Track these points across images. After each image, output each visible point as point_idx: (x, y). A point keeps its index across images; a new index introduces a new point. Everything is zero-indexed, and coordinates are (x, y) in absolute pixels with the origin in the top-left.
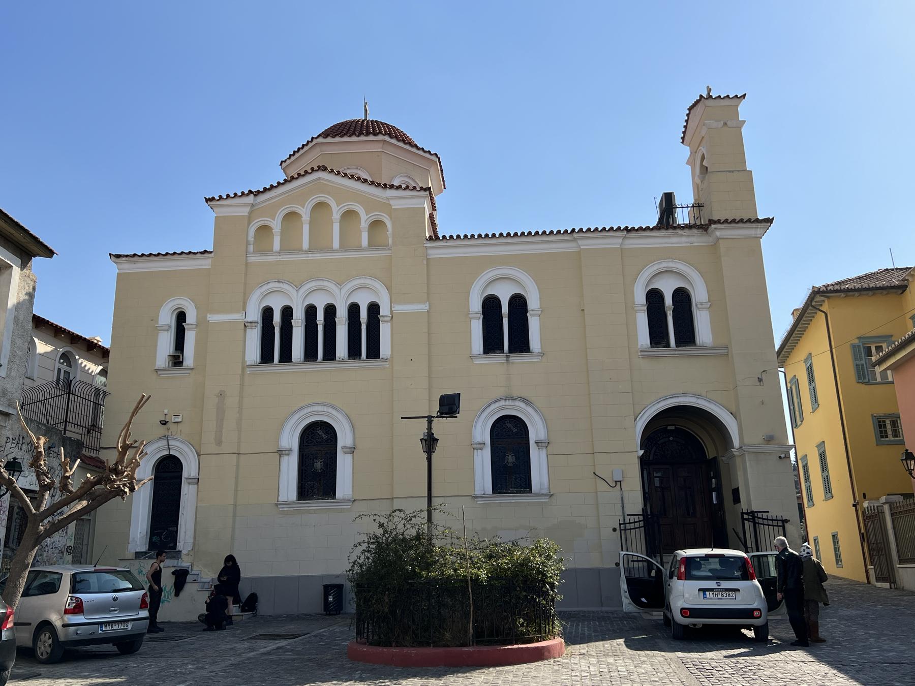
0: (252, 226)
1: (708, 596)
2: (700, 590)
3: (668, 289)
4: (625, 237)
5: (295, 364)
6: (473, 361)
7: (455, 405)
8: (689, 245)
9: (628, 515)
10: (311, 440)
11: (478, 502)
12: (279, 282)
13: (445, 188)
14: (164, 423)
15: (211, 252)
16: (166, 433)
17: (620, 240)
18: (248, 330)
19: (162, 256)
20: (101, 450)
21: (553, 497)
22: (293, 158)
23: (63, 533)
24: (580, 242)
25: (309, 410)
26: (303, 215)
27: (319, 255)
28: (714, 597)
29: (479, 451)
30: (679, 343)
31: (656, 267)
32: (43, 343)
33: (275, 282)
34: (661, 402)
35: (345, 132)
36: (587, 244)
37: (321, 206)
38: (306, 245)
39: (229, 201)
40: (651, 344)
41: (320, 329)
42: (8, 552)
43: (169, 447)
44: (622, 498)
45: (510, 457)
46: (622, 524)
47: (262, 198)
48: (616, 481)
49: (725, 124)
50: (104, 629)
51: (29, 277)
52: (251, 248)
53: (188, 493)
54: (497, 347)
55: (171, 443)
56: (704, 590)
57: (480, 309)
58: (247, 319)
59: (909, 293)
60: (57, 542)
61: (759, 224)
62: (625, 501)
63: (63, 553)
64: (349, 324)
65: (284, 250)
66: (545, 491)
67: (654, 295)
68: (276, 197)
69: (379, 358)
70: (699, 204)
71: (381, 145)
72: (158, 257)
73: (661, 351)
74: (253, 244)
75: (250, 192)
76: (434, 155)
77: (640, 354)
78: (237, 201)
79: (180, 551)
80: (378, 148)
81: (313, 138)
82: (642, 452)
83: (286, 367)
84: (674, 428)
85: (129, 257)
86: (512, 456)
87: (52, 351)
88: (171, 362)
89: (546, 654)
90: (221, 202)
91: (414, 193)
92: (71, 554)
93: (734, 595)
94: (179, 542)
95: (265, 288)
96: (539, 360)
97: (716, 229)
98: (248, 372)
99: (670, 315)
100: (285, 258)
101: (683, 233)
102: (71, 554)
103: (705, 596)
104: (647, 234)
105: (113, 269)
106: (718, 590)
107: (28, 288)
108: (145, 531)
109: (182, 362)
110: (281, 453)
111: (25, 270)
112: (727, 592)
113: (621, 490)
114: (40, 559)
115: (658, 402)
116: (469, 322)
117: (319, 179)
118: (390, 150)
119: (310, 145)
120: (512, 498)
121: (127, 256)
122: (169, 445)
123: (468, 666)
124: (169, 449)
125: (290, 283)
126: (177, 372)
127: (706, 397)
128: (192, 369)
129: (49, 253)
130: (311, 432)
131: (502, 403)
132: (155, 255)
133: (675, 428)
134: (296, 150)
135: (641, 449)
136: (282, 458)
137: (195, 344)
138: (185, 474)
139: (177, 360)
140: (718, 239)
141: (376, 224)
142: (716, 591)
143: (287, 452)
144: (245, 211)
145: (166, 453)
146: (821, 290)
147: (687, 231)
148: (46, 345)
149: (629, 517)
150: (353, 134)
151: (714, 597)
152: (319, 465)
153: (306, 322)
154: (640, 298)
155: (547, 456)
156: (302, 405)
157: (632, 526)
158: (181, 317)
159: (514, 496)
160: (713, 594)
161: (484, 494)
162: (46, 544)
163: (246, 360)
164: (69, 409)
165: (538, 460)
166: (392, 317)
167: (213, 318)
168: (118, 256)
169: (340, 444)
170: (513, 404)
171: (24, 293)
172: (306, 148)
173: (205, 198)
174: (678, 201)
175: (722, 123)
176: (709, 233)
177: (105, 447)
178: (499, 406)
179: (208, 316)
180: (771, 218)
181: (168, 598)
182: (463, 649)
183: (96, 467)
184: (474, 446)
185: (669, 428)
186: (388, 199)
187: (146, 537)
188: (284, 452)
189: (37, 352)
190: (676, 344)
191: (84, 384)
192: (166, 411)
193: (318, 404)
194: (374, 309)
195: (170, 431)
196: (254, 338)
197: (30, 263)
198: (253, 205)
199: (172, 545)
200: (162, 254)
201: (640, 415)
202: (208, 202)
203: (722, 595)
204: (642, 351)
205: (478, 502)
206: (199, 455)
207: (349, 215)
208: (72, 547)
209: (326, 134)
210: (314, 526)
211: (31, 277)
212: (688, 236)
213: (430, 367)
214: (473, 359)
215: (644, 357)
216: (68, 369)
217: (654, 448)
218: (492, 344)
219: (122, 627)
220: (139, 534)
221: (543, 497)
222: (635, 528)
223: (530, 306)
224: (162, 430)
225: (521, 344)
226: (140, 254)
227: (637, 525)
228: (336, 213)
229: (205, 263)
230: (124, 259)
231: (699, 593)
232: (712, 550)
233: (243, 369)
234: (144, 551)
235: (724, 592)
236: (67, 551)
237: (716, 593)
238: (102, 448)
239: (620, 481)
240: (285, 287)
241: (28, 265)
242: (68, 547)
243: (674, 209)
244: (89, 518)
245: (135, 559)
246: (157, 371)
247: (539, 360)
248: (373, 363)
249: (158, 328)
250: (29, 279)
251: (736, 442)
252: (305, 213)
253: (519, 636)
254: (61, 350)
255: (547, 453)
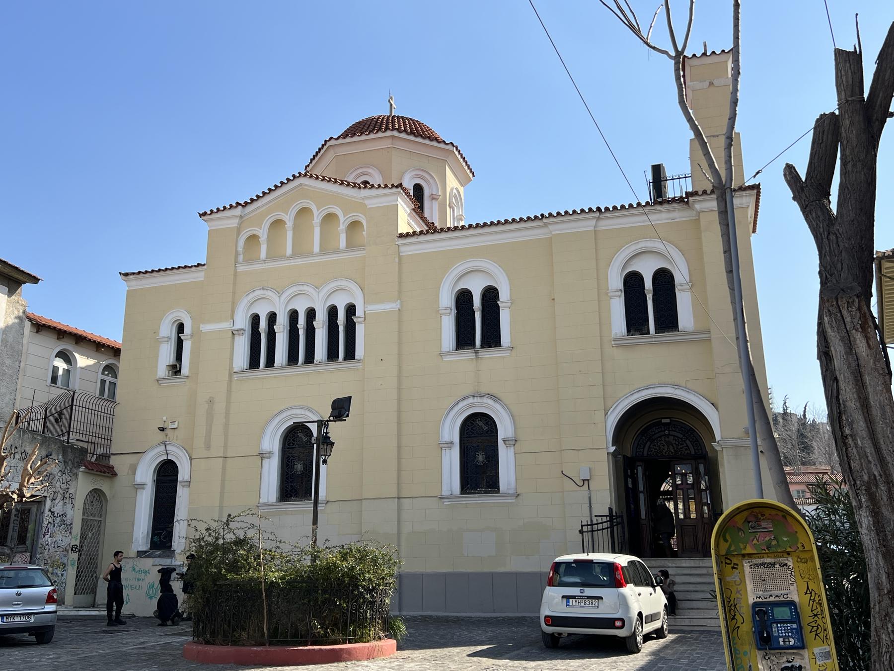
0: (243, 235)
1: (571, 604)
2: (563, 597)
3: (647, 271)
4: (599, 219)
5: (278, 368)
6: (443, 359)
7: (344, 408)
8: (670, 221)
9: (596, 516)
10: (471, 431)
11: (445, 503)
12: (263, 289)
13: (474, 176)
14: (162, 429)
15: (204, 265)
16: (165, 439)
17: (593, 222)
18: (236, 338)
19: (182, 269)
20: (112, 457)
21: (519, 497)
22: (314, 162)
23: (66, 533)
24: (551, 227)
25: (289, 413)
26: (287, 222)
27: (299, 260)
28: (577, 605)
29: (447, 450)
30: (660, 328)
31: (633, 248)
32: (85, 357)
33: (260, 289)
34: (634, 395)
35: (371, 130)
36: (558, 228)
37: (304, 211)
38: (289, 251)
39: (220, 215)
40: (629, 330)
41: (341, 329)
42: (6, 550)
43: (167, 452)
44: (590, 498)
45: (480, 456)
46: (584, 525)
47: (250, 208)
48: (583, 480)
49: (711, 84)
50: (5, 621)
51: (18, 303)
52: (241, 258)
53: (182, 494)
54: (470, 342)
55: (168, 448)
56: (567, 598)
57: (621, 286)
58: (234, 328)
59: (58, 344)
60: (60, 542)
61: (744, 193)
62: (592, 502)
63: (67, 551)
64: (329, 326)
65: (271, 257)
66: (511, 492)
67: (634, 279)
68: (263, 206)
69: (355, 359)
70: (685, 175)
71: (390, 141)
72: (153, 274)
73: (638, 338)
74: (243, 254)
75: (238, 204)
76: (451, 145)
77: (613, 343)
78: (227, 213)
79: (174, 551)
80: (387, 144)
81: (326, 141)
82: (612, 449)
83: (270, 372)
84: (669, 421)
85: (135, 275)
86: (482, 455)
87: (94, 364)
88: (171, 372)
89: (345, 656)
90: (213, 216)
91: (387, 191)
92: (76, 552)
93: (597, 604)
94: (174, 542)
95: (252, 295)
96: (508, 354)
97: (694, 201)
98: (236, 378)
99: (649, 299)
100: (269, 266)
101: (662, 209)
102: (76, 552)
103: (568, 604)
104: (566, 219)
105: (123, 287)
106: (580, 597)
107: (17, 313)
108: (146, 531)
109: (180, 371)
110: (263, 456)
111: (13, 297)
112: (590, 600)
113: (589, 489)
114: (40, 557)
115: (631, 395)
116: (439, 319)
117: (301, 185)
118: (400, 145)
119: (325, 148)
120: (478, 499)
121: (133, 274)
122: (166, 451)
123: (255, 665)
124: (167, 454)
125: (273, 289)
126: (176, 380)
127: (685, 388)
128: (187, 377)
129: (35, 280)
130: (471, 423)
131: (470, 400)
132: (156, 271)
133: (670, 420)
134: (318, 151)
135: (613, 446)
136: (264, 460)
137: (191, 353)
138: (180, 478)
139: (176, 370)
140: (699, 213)
141: (354, 225)
142: (578, 599)
143: (267, 455)
144: (234, 223)
145: (164, 457)
146: (886, 255)
147: (675, 205)
148: (87, 358)
149: (597, 518)
150: (380, 130)
151: (577, 605)
152: (299, 467)
153: (290, 327)
154: (616, 282)
155: (515, 454)
156: (282, 408)
157: (600, 526)
158: (181, 328)
159: (479, 497)
160: (576, 602)
161: (451, 495)
162: (47, 543)
163: (234, 366)
164: (73, 418)
165: (505, 456)
166: (365, 317)
167: (206, 328)
168: (127, 275)
169: (501, 435)
170: (481, 401)
171: (13, 317)
172: (322, 151)
173: (199, 213)
174: (668, 173)
175: (707, 83)
176: (690, 206)
177: (115, 453)
178: (467, 403)
179: (201, 326)
180: (757, 184)
181: (155, 594)
182: (252, 649)
183: (101, 472)
184: (442, 446)
185: (664, 421)
186: (363, 198)
187: (147, 538)
188: (264, 455)
189: (78, 366)
190: (655, 330)
191: (91, 397)
192: (164, 418)
193: (296, 408)
194: (351, 310)
195: (168, 437)
196: (242, 345)
197: (19, 290)
198: (241, 217)
199: (168, 545)
200: (169, 269)
201: (612, 409)
202: (202, 217)
203: (585, 603)
204: (615, 340)
205: (445, 503)
206: (191, 459)
207: (330, 218)
208: (77, 546)
209: (345, 135)
210: (291, 527)
211: (20, 302)
212: (669, 211)
213: (400, 366)
214: (443, 357)
215: (618, 346)
216: (113, 380)
217: (649, 443)
218: (464, 339)
219: (24, 620)
220: (141, 534)
221: (509, 498)
222: (603, 529)
223: (678, 279)
224: (161, 436)
225: (492, 338)
226: (170, 268)
227: (605, 525)
228: (317, 218)
229: (198, 276)
230: (131, 277)
231: (562, 600)
232: (588, 555)
233: (230, 375)
234: (145, 550)
235: (587, 600)
236: (72, 550)
237: (579, 600)
238: (112, 454)
239: (588, 480)
240: (269, 294)
241: (17, 292)
242: (73, 546)
243: (662, 182)
244: (100, 519)
245: (137, 557)
246: (158, 381)
247: (508, 354)
248: (350, 364)
249: (160, 340)
250: (18, 304)
251: (718, 438)
252: (289, 219)
253: (317, 638)
254: (104, 362)
255: (514, 452)
